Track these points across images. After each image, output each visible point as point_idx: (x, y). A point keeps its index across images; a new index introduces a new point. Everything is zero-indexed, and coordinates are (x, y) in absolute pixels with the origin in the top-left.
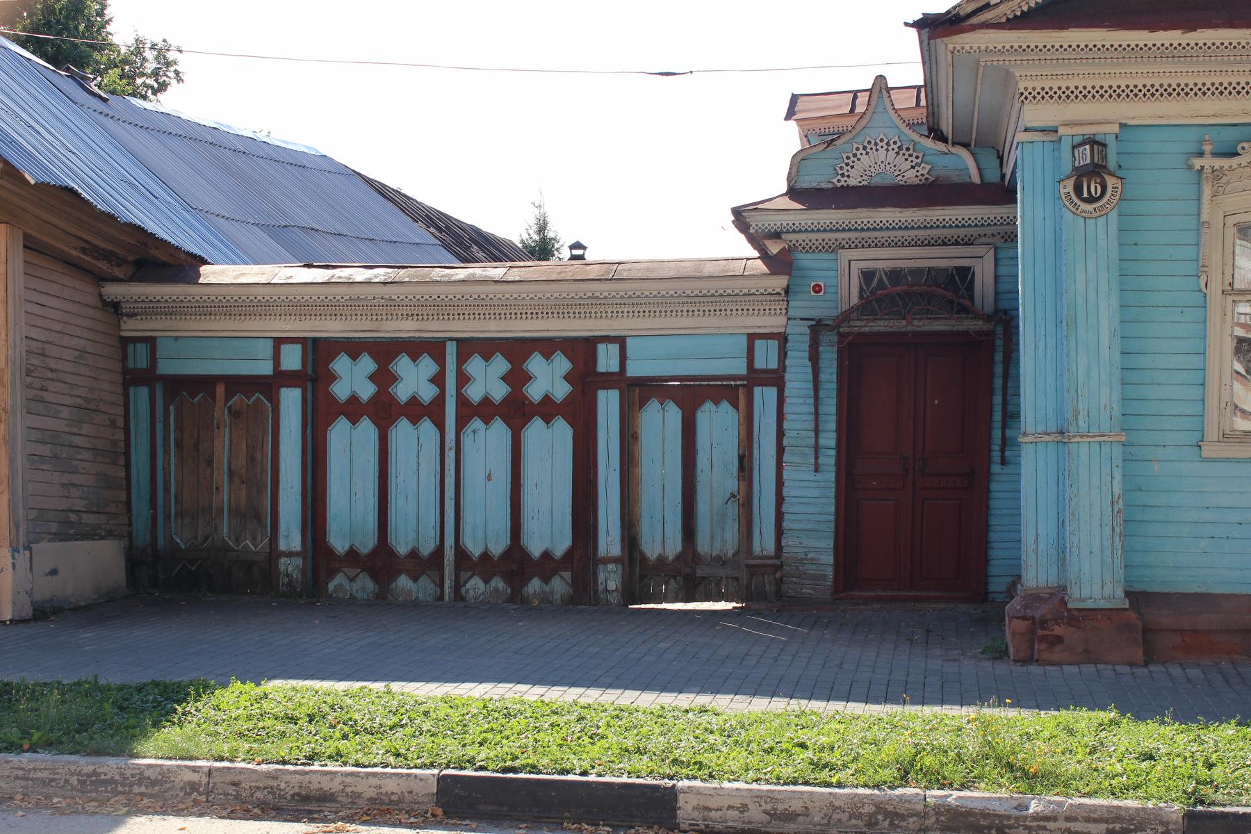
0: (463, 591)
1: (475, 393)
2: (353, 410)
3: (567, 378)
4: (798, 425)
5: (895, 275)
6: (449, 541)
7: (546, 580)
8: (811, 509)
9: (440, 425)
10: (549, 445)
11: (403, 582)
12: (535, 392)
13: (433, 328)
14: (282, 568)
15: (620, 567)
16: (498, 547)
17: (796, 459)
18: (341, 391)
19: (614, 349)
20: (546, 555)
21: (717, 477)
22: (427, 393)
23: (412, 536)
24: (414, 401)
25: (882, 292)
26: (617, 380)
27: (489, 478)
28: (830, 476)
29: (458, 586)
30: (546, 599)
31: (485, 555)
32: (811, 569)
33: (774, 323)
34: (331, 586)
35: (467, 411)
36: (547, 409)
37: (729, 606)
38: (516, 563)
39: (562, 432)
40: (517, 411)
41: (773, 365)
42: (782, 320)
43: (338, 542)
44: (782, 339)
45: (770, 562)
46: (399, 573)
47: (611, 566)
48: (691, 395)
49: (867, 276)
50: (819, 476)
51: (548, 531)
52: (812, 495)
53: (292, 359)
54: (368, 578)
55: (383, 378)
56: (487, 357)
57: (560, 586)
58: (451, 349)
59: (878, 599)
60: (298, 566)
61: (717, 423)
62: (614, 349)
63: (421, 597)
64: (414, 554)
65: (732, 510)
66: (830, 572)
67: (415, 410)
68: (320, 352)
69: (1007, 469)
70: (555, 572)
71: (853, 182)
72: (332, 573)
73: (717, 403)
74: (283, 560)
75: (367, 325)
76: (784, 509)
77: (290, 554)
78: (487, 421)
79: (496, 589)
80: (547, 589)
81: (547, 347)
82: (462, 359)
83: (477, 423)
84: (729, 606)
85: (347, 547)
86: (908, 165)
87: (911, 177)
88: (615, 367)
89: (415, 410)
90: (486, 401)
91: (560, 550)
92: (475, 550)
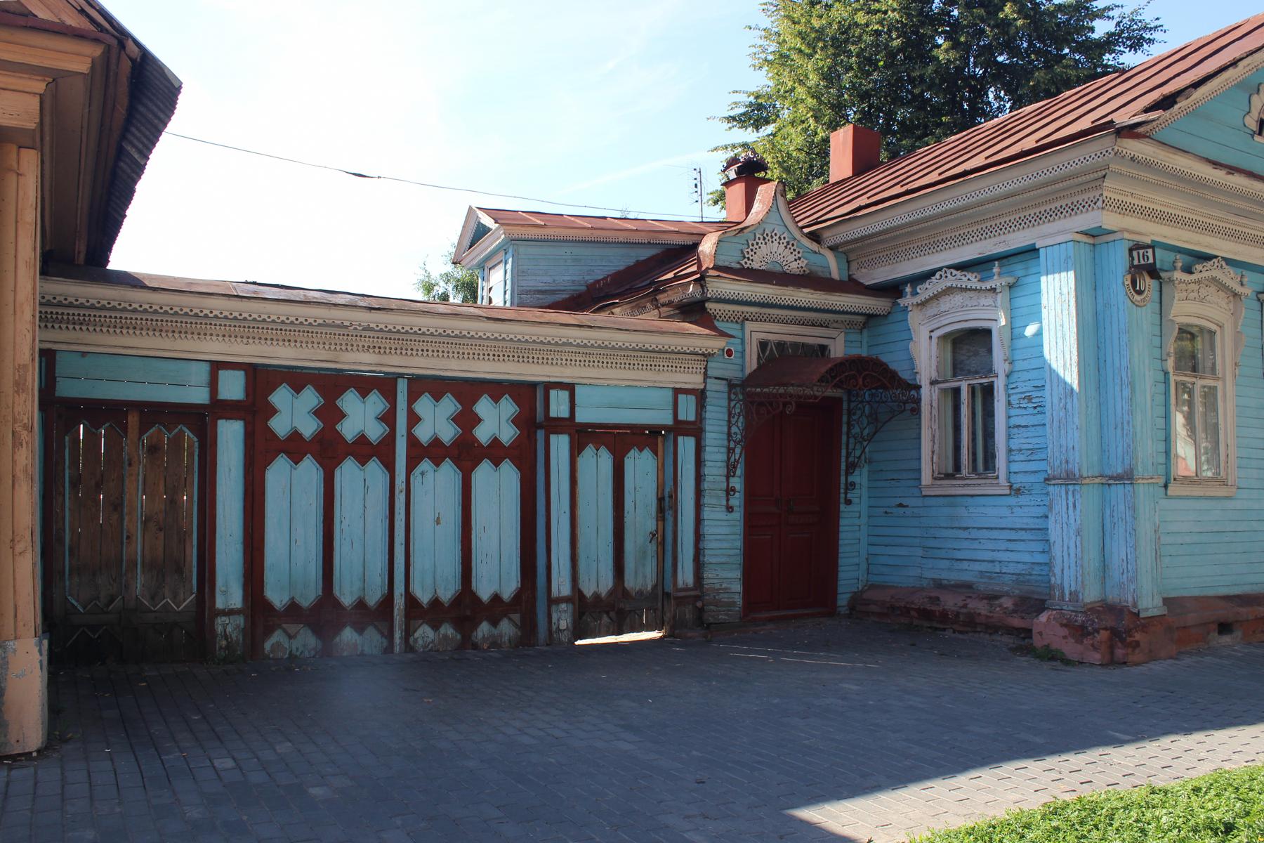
0: (411, 639)
1: (424, 433)
2: (295, 447)
3: (273, 411)
4: (715, 471)
5: (781, 345)
6: (399, 589)
7: (495, 623)
8: (725, 545)
9: (390, 466)
10: (497, 487)
11: (348, 635)
12: (483, 434)
13: (394, 363)
14: (219, 629)
15: (570, 606)
16: (447, 592)
17: (714, 501)
18: (280, 426)
19: (564, 395)
20: (496, 598)
21: (641, 518)
22: (375, 432)
23: (358, 584)
24: (362, 439)
25: (777, 358)
26: (567, 425)
27: (438, 521)
28: (738, 515)
29: (408, 633)
30: (495, 643)
31: (436, 602)
32: (724, 598)
33: (693, 380)
34: (268, 646)
35: (417, 452)
36: (496, 452)
37: (655, 634)
38: (465, 608)
39: (509, 475)
40: (466, 453)
41: (692, 417)
42: (700, 378)
43: (276, 595)
44: (701, 396)
45: (692, 593)
46: (343, 626)
47: (563, 606)
48: (621, 440)
49: (763, 345)
50: (731, 516)
51: (497, 574)
52: (725, 530)
53: (233, 387)
54: (309, 633)
55: (329, 414)
56: (437, 397)
57: (507, 628)
58: (402, 386)
59: (771, 620)
60: (238, 626)
61: (640, 466)
62: (564, 395)
63: (367, 650)
64: (361, 604)
65: (652, 548)
66: (739, 600)
67: (363, 450)
68: (262, 379)
69: (850, 508)
70: (505, 615)
71: (756, 266)
72: (269, 631)
73: (641, 450)
74: (220, 620)
75: (323, 355)
76: (701, 546)
77: (230, 613)
78: (437, 463)
79: (445, 636)
80: (496, 632)
81: (496, 389)
82: (413, 397)
83: (426, 465)
84: (655, 634)
85: (286, 599)
86: (791, 258)
87: (794, 267)
88: (565, 413)
89: (363, 450)
90: (436, 442)
91: (508, 592)
92: (424, 597)
